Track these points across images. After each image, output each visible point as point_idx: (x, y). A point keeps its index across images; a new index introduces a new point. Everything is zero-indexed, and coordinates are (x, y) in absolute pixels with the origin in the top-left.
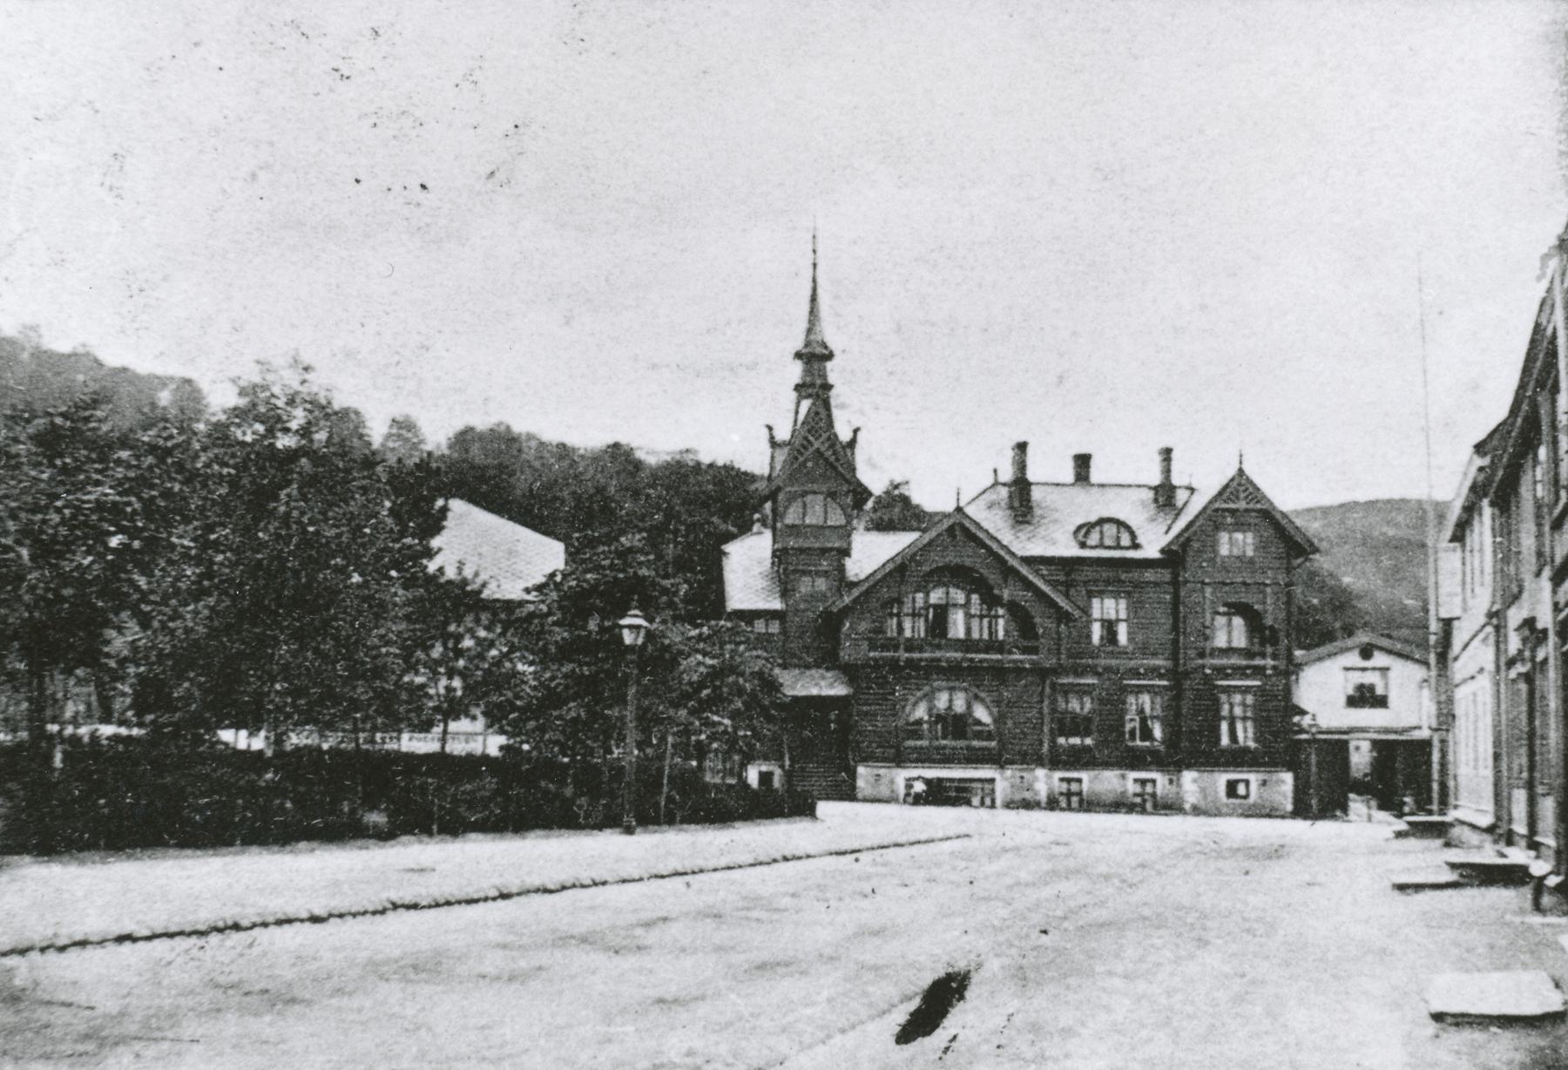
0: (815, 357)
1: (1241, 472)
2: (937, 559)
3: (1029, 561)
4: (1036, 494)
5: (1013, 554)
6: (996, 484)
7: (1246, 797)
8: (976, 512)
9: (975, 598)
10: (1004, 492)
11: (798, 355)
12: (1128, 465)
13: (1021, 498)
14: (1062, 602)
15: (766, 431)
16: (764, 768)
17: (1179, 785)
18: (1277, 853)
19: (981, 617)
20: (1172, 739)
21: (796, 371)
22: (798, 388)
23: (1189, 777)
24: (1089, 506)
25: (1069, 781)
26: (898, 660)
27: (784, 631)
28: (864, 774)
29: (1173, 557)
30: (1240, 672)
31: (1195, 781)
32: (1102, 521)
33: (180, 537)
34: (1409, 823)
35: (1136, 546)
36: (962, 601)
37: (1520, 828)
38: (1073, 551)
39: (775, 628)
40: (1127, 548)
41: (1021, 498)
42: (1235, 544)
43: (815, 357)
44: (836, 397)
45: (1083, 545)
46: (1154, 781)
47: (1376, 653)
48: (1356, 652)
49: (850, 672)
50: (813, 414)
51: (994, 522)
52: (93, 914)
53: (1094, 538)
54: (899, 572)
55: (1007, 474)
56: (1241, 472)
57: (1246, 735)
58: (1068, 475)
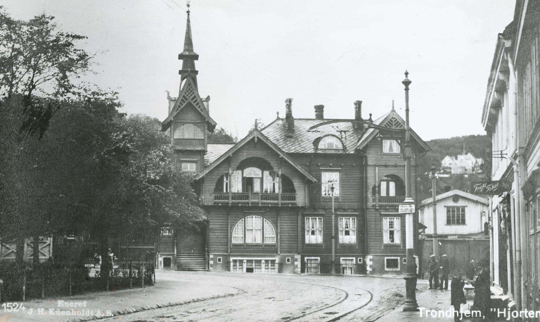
0: (189, 58)
1: (393, 111)
2: (244, 156)
4: (296, 123)
5: (282, 152)
6: (278, 119)
11: (181, 57)
12: (341, 109)
13: (289, 125)
15: (167, 93)
21: (180, 64)
22: (180, 72)
26: (228, 203)
33: (170, 208)
34: (214, 255)
37: (444, 286)
41: (289, 125)
42: (390, 146)
43: (189, 58)
44: (199, 78)
50: (188, 84)
52: (11, 308)
54: (227, 161)
55: (283, 115)
56: (393, 111)
58: (313, 115)
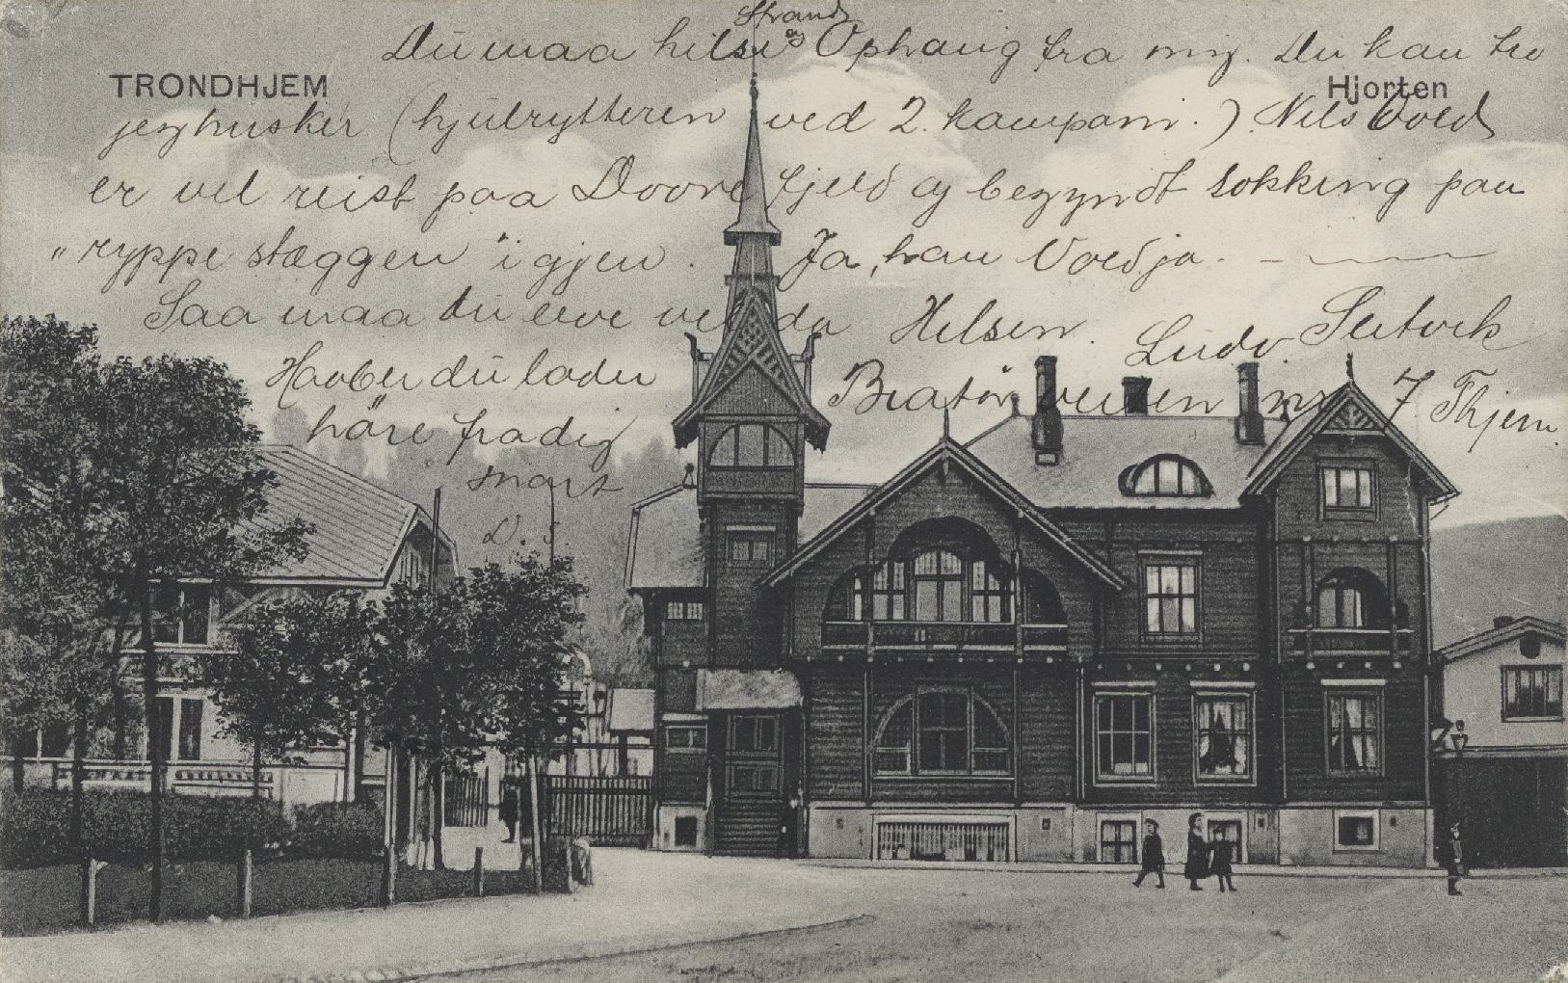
3: (1060, 515)
7: (1370, 841)
8: (988, 455)
9: (979, 568)
10: (1024, 427)
13: (1048, 429)
14: (1102, 572)
16: (683, 812)
17: (1277, 829)
18: (1516, 150)
19: (986, 593)
20: (1266, 762)
23: (1288, 818)
24: (1138, 439)
25: (1117, 824)
27: (711, 615)
28: (818, 819)
29: (1256, 506)
30: (1354, 667)
31: (1294, 821)
32: (1156, 461)
35: (1206, 491)
36: (957, 571)
38: (1118, 501)
39: (696, 611)
40: (1195, 495)
41: (1048, 429)
45: (1129, 493)
46: (1238, 824)
47: (1545, 649)
48: (1517, 646)
49: (805, 674)
51: (1009, 462)
53: (1146, 483)
57: (1366, 752)
58: (1116, 404)
